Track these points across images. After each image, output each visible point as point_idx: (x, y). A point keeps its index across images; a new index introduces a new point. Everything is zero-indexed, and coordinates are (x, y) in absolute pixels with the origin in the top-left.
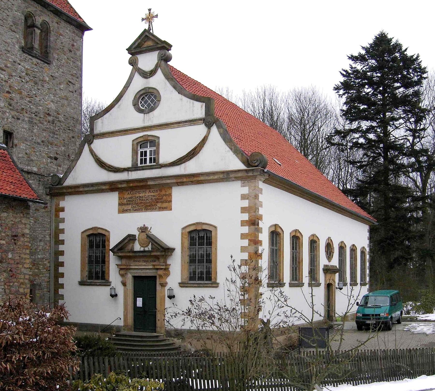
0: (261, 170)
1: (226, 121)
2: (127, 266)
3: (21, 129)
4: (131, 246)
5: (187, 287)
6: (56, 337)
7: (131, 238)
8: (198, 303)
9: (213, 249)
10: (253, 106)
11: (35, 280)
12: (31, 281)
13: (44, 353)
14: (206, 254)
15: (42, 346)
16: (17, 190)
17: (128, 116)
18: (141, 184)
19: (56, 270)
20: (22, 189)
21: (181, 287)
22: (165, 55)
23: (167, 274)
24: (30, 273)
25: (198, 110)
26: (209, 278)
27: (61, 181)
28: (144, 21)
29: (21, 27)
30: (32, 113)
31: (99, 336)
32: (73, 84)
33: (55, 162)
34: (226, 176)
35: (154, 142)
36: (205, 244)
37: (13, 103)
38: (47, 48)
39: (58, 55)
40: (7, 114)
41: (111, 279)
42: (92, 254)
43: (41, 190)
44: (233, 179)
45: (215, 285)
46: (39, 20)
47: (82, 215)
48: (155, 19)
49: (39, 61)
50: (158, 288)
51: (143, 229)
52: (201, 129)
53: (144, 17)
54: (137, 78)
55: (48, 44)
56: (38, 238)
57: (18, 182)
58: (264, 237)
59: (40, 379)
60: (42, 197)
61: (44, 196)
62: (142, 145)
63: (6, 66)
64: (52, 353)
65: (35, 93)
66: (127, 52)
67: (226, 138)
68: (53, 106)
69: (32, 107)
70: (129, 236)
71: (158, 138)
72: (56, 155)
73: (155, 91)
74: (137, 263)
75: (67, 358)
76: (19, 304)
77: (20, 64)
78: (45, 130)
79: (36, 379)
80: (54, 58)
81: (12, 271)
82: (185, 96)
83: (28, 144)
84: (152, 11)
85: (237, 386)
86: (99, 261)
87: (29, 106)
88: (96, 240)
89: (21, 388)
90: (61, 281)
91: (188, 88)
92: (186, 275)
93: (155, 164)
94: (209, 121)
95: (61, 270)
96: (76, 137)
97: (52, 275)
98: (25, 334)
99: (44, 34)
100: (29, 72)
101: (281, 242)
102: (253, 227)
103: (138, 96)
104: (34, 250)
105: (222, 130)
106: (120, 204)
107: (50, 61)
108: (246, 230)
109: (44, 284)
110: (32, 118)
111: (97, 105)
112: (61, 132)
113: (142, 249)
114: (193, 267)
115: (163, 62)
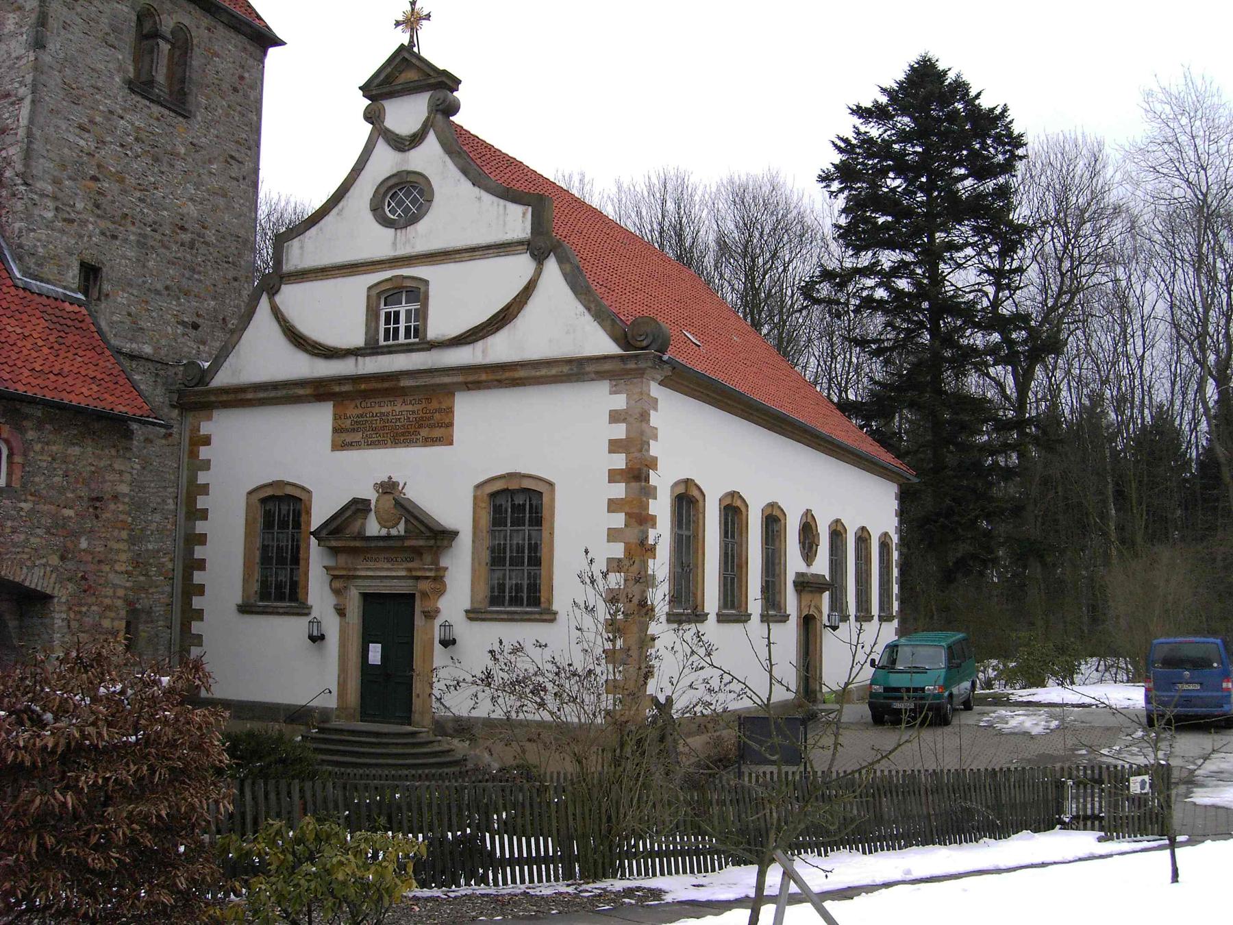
0: (655, 356)
3: (119, 260)
4: (358, 523)
6: (181, 733)
7: (360, 506)
8: (509, 657)
9: (545, 534)
10: (639, 214)
12: (129, 603)
14: (530, 544)
15: (150, 753)
18: (386, 385)
19: (188, 577)
20: (118, 393)
21: (471, 619)
23: (441, 591)
25: (515, 222)
26: (535, 600)
27: (204, 377)
29: (129, 36)
31: (280, 731)
33: (192, 333)
34: (573, 370)
35: (417, 292)
39: (208, 98)
40: (91, 227)
41: (310, 601)
43: (159, 396)
45: (549, 616)
46: (168, 23)
47: (256, 452)
48: (424, 22)
49: (167, 112)
50: (419, 621)
51: (388, 488)
52: (523, 265)
53: (401, 18)
54: (382, 148)
58: (661, 508)
63: (92, 121)
64: (172, 770)
68: (192, 210)
70: (355, 501)
71: (426, 282)
72: (195, 319)
73: (421, 180)
74: (371, 564)
76: (99, 654)
78: (174, 264)
79: (133, 830)
80: (198, 105)
82: (488, 190)
84: (418, 6)
88: (279, 510)
92: (484, 591)
93: (417, 340)
94: (539, 246)
95: (198, 577)
96: (243, 279)
97: (178, 590)
98: (110, 725)
99: (178, 53)
100: (143, 135)
102: (634, 484)
103: (382, 190)
105: (568, 267)
106: (336, 430)
108: (619, 490)
109: (159, 610)
110: (145, 236)
113: (384, 532)
114: (498, 574)
115: (439, 117)
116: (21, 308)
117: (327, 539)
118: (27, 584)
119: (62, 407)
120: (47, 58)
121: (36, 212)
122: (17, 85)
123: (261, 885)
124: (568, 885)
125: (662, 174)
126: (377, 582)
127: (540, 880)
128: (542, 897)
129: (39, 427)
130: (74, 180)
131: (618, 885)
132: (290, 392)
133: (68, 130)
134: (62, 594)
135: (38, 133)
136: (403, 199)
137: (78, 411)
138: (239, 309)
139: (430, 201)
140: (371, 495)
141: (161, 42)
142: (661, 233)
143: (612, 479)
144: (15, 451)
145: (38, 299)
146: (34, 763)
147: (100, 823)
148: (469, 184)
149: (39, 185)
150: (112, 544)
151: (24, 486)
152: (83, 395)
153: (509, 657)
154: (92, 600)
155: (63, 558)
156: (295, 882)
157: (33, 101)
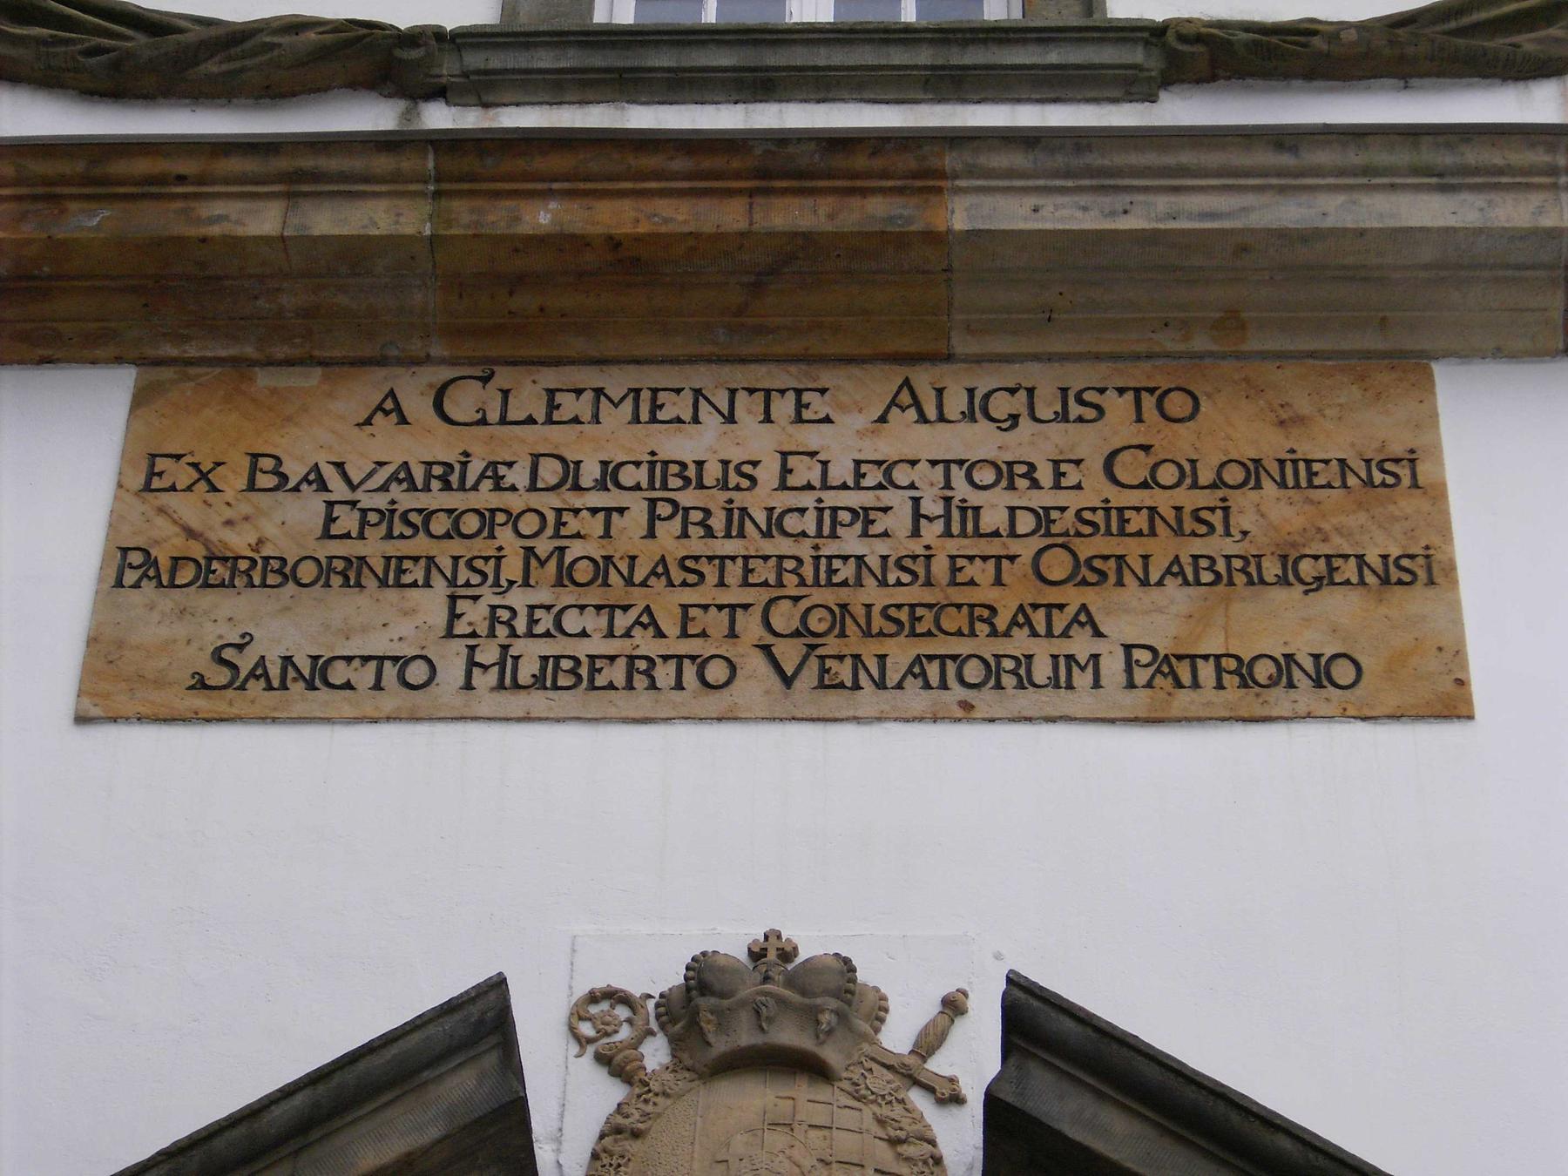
106: (132, 566)
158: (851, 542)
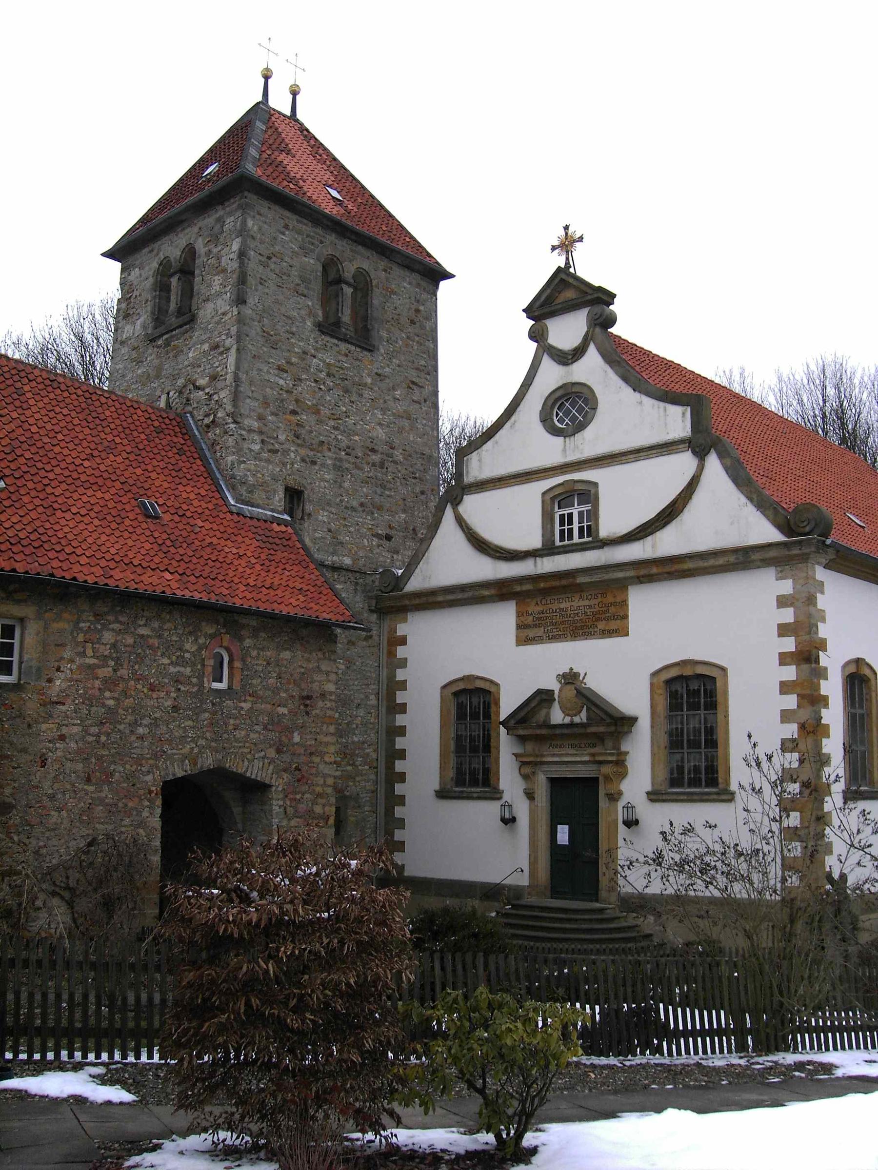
0: (818, 541)
1: (739, 441)
2: (537, 756)
3: (319, 483)
4: (543, 712)
5: (664, 801)
6: (368, 910)
7: (544, 697)
8: (680, 837)
9: (720, 717)
10: (800, 402)
11: (347, 787)
12: (338, 790)
13: (342, 942)
14: (706, 728)
15: (340, 928)
16: (312, 605)
17: (533, 445)
18: (564, 582)
19: (390, 766)
20: (322, 602)
21: (652, 800)
22: (601, 315)
23: (623, 774)
24: (338, 773)
25: (676, 422)
26: (713, 782)
27: (398, 583)
28: (557, 251)
29: (317, 286)
30: (340, 449)
31: (473, 907)
32: (419, 386)
33: (385, 542)
34: (740, 559)
35: (588, 494)
36: (702, 707)
37: (303, 432)
38: (366, 321)
39: (389, 332)
40: (292, 455)
41: (502, 786)
42: (464, 733)
43: (359, 603)
44: (759, 563)
45: (727, 796)
46: (349, 269)
47: (450, 649)
48: (577, 244)
49: (353, 348)
50: (603, 803)
51: (570, 678)
52: (683, 464)
53: (556, 243)
54: (547, 363)
55: (369, 312)
56: (352, 701)
57: (312, 589)
58: (833, 687)
59: (333, 997)
60: (362, 617)
61: (366, 615)
62: (562, 503)
63: (289, 362)
64: (359, 943)
65: (344, 409)
66: (525, 315)
67: (741, 478)
68: (380, 433)
69: (340, 437)
70: (539, 692)
71: (596, 485)
72: (388, 531)
73: (585, 390)
74: (556, 751)
75: (391, 955)
76: (296, 840)
77: (314, 357)
78: (367, 483)
79: (326, 996)
80: (381, 338)
81: (300, 770)
82: (649, 394)
83: (333, 510)
84: (571, 230)
85: (767, 1027)
86: (478, 746)
87: (333, 437)
88: (471, 702)
89: (294, 1013)
90: (399, 789)
91: (653, 378)
92: (663, 774)
93: (590, 539)
94: (700, 444)
95: (399, 766)
96: (429, 493)
97: (382, 776)
98: (305, 902)
99: (360, 295)
100: (334, 370)
101: (871, 697)
102: (805, 667)
103: (550, 403)
104: (345, 726)
105: (728, 461)
106: (519, 627)
107: (374, 346)
108: (790, 673)
109: (365, 797)
110: (340, 460)
111: (471, 423)
112: (398, 484)
113: (567, 720)
114: (678, 757)
115: (598, 330)
116: (236, 531)
117: (515, 728)
118: (248, 774)
119: (273, 616)
120: (247, 311)
121: (246, 446)
122: (224, 337)
123: (439, 1047)
124: (741, 1058)
125: (820, 362)
126: (563, 768)
127: (713, 1051)
128: (714, 1068)
129: (255, 636)
130: (276, 415)
131: (790, 1058)
132: (477, 593)
133: (268, 372)
134: (279, 783)
135: (243, 377)
136: (570, 409)
137: (289, 620)
138: (427, 519)
139: (595, 409)
140: (554, 685)
141: (344, 286)
142: (823, 418)
143: (782, 663)
144: (235, 658)
145: (250, 522)
146: (241, 935)
147: (299, 989)
148: (630, 390)
149: (247, 422)
150: (321, 738)
151: (243, 687)
152: (291, 605)
153: (680, 837)
154: (305, 788)
155: (279, 751)
156: (469, 1046)
157: (238, 349)
158: (577, 618)
